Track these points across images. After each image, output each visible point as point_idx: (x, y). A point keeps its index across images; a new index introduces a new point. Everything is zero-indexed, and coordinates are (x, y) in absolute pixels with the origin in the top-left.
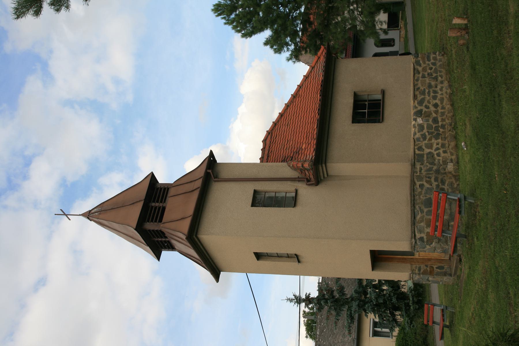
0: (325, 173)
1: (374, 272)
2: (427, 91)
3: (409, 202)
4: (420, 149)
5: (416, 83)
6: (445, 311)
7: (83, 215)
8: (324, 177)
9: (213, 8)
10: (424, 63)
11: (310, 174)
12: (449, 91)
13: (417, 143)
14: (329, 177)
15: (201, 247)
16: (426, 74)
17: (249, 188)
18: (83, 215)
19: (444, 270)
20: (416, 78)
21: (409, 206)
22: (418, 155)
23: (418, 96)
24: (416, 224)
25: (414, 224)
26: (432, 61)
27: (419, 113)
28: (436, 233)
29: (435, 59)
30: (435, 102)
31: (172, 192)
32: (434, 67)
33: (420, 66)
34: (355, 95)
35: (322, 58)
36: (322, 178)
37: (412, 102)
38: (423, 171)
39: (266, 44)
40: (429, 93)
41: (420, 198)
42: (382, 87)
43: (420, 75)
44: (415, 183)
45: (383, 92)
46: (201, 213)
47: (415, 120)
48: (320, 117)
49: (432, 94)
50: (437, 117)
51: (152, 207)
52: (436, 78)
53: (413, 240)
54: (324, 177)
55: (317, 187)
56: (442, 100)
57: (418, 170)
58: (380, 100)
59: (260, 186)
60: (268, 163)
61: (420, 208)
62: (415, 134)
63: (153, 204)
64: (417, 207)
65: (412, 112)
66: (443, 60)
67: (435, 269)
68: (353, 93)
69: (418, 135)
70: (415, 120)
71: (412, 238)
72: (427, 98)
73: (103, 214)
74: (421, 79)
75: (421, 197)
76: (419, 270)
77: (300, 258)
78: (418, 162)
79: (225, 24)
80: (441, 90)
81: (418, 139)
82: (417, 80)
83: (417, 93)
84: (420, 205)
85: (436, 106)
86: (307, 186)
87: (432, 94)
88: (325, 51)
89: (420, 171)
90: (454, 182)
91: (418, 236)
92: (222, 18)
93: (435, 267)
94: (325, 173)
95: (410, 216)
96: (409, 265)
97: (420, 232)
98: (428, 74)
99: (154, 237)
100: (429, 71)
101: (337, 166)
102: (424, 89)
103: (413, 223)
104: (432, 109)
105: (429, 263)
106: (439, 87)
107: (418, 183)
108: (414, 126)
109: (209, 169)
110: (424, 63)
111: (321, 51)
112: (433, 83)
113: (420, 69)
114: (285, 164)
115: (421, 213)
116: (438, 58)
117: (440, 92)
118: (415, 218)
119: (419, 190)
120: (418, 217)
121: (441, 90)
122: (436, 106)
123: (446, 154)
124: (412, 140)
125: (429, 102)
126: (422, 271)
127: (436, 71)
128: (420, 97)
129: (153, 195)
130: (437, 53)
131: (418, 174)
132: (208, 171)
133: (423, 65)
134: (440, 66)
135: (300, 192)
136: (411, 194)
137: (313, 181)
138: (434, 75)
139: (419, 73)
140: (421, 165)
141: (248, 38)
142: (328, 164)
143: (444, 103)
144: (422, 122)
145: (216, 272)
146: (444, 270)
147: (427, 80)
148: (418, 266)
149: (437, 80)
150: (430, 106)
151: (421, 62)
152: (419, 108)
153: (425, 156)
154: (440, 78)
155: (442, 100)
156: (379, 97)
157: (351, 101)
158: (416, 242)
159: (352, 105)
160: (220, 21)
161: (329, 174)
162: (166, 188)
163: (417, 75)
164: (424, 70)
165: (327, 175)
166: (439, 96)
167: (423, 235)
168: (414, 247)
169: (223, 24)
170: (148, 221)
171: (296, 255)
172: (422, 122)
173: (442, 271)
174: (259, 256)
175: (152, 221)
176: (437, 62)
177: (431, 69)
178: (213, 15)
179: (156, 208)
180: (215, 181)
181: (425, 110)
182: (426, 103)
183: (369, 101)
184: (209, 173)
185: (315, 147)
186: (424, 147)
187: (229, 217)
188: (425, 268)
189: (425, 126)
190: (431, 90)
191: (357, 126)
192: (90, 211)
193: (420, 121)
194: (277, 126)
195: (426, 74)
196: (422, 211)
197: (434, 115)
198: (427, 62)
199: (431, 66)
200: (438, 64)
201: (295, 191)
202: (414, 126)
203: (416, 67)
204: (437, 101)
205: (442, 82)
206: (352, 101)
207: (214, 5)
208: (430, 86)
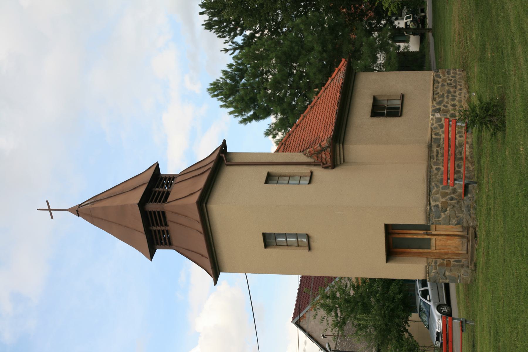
0: (342, 157)
1: (389, 264)
2: (446, 95)
3: (425, 181)
4: (436, 134)
5: (435, 90)
6: (464, 324)
7: (70, 210)
8: (340, 163)
9: (209, 87)
10: (444, 76)
11: (326, 156)
12: (467, 96)
13: (434, 130)
14: (344, 162)
15: (208, 223)
16: (446, 84)
17: (264, 171)
18: (70, 210)
19: (461, 263)
20: (435, 86)
21: (425, 183)
22: (435, 139)
23: (437, 98)
24: (431, 196)
25: (430, 195)
26: (452, 75)
27: (438, 110)
28: (449, 181)
29: (455, 73)
30: (453, 103)
31: (178, 179)
32: (453, 79)
33: (440, 78)
34: (375, 99)
35: (342, 69)
36: (339, 163)
37: (431, 102)
38: (439, 156)
39: (267, 134)
40: (448, 97)
41: (436, 178)
42: (403, 92)
43: (440, 84)
44: (432, 167)
45: (403, 97)
46: (214, 183)
47: (434, 115)
48: (339, 108)
49: (450, 97)
50: (455, 114)
51: (156, 192)
52: (455, 87)
53: (428, 207)
54: (340, 163)
55: (334, 170)
56: (460, 101)
57: (435, 154)
58: (399, 108)
59: (273, 169)
60: (284, 153)
61: (436, 185)
62: (433, 124)
63: (157, 189)
64: (433, 184)
65: (431, 110)
66: (462, 74)
67: (452, 262)
68: (372, 97)
69: (435, 125)
70: (434, 115)
71: (427, 205)
72: (446, 99)
73: (92, 211)
74: (440, 87)
75: (437, 177)
76: (436, 263)
77: (311, 240)
78: (435, 143)
79: (222, 106)
80: (460, 94)
81: (436, 128)
82: (437, 88)
83: (436, 96)
84: (436, 183)
85: (454, 105)
86: (323, 169)
87: (450, 97)
88: (346, 62)
89: (437, 156)
90: (470, 166)
91: (433, 203)
92: (219, 99)
93: (452, 260)
94: (342, 157)
95: (425, 190)
96: (425, 259)
97: (435, 201)
98: (448, 84)
99: (153, 225)
100: (449, 82)
101: (356, 148)
102: (443, 94)
103: (429, 181)
104: (450, 107)
105: (446, 256)
106: (457, 93)
107: (434, 168)
108: (432, 119)
109: (222, 153)
110: (444, 76)
111: (341, 64)
112: (452, 90)
113: (440, 80)
114: (301, 153)
115: (437, 188)
116: (458, 72)
117: (458, 96)
118: (430, 191)
119: (436, 172)
120: (434, 191)
121: (460, 94)
122: (454, 105)
123: (462, 138)
124: (430, 130)
125: (447, 103)
126: (438, 263)
127: (455, 81)
128: (438, 100)
129: (156, 184)
130: (457, 70)
131: (435, 160)
132: (221, 155)
133: (443, 78)
134: (460, 78)
135: (315, 173)
136: (427, 175)
137: (329, 164)
138: (453, 84)
139: (439, 83)
140: (437, 147)
141: (248, 123)
142: (345, 146)
143: (462, 104)
144: (439, 116)
145: (215, 272)
146: (461, 263)
147: (447, 88)
148: (434, 260)
149: (456, 88)
150: (449, 105)
151: (441, 75)
152: (438, 107)
153: (442, 140)
154: (459, 87)
155: (460, 101)
156: (398, 103)
157: (371, 102)
158: (430, 208)
159: (371, 105)
160: (217, 102)
161: (346, 161)
162: (171, 178)
163: (436, 85)
164: (444, 81)
165: (344, 162)
166: (457, 99)
167: (437, 203)
168: (428, 215)
169: (219, 106)
170: (151, 202)
171: (307, 234)
172: (439, 116)
173: (459, 264)
174: (268, 240)
175: (155, 202)
176: (457, 76)
177: (451, 80)
178: (208, 96)
179: (159, 192)
180: (227, 165)
181: (442, 108)
182: (444, 103)
183: (388, 108)
184: (222, 157)
185: (333, 128)
186: (441, 133)
187: (236, 208)
188: (442, 261)
189: (443, 119)
190: (450, 95)
191: (376, 120)
192: (80, 205)
193: (438, 115)
194: (291, 136)
195: (446, 84)
196: (437, 187)
197: (452, 112)
198: (447, 76)
199: (451, 78)
200: (458, 77)
201: (310, 175)
202: (432, 119)
203: (436, 78)
204: (455, 102)
205: (461, 89)
206: (372, 102)
207: (211, 84)
208: (449, 92)
